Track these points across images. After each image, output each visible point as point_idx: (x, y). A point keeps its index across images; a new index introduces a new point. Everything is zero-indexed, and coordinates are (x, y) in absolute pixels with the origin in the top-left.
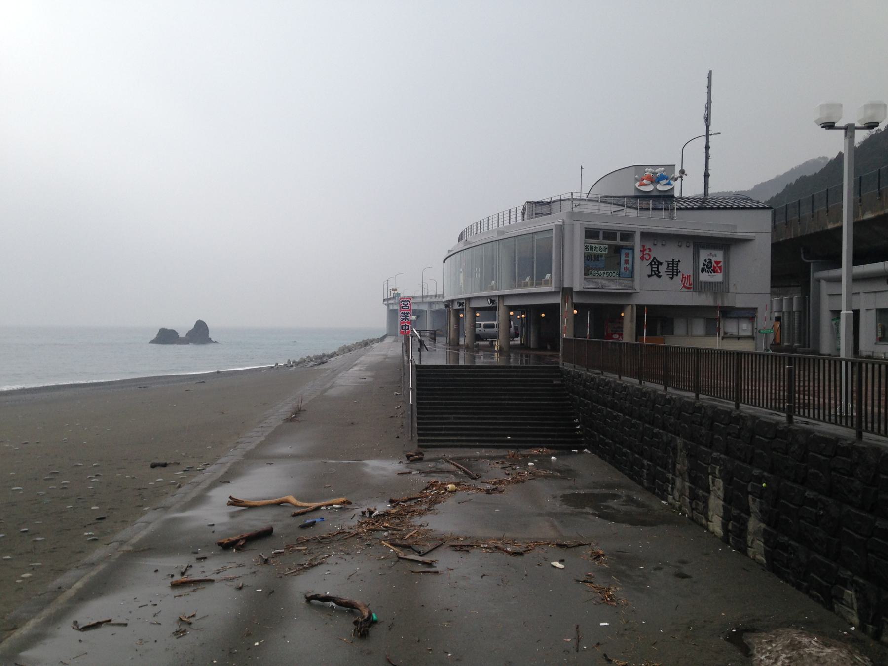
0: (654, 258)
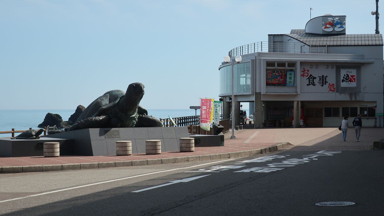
0: (311, 75)
